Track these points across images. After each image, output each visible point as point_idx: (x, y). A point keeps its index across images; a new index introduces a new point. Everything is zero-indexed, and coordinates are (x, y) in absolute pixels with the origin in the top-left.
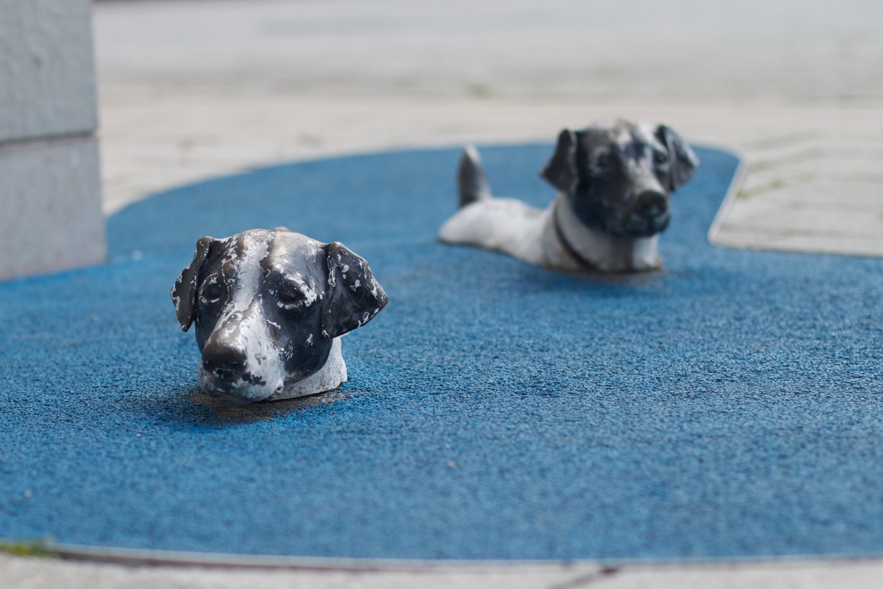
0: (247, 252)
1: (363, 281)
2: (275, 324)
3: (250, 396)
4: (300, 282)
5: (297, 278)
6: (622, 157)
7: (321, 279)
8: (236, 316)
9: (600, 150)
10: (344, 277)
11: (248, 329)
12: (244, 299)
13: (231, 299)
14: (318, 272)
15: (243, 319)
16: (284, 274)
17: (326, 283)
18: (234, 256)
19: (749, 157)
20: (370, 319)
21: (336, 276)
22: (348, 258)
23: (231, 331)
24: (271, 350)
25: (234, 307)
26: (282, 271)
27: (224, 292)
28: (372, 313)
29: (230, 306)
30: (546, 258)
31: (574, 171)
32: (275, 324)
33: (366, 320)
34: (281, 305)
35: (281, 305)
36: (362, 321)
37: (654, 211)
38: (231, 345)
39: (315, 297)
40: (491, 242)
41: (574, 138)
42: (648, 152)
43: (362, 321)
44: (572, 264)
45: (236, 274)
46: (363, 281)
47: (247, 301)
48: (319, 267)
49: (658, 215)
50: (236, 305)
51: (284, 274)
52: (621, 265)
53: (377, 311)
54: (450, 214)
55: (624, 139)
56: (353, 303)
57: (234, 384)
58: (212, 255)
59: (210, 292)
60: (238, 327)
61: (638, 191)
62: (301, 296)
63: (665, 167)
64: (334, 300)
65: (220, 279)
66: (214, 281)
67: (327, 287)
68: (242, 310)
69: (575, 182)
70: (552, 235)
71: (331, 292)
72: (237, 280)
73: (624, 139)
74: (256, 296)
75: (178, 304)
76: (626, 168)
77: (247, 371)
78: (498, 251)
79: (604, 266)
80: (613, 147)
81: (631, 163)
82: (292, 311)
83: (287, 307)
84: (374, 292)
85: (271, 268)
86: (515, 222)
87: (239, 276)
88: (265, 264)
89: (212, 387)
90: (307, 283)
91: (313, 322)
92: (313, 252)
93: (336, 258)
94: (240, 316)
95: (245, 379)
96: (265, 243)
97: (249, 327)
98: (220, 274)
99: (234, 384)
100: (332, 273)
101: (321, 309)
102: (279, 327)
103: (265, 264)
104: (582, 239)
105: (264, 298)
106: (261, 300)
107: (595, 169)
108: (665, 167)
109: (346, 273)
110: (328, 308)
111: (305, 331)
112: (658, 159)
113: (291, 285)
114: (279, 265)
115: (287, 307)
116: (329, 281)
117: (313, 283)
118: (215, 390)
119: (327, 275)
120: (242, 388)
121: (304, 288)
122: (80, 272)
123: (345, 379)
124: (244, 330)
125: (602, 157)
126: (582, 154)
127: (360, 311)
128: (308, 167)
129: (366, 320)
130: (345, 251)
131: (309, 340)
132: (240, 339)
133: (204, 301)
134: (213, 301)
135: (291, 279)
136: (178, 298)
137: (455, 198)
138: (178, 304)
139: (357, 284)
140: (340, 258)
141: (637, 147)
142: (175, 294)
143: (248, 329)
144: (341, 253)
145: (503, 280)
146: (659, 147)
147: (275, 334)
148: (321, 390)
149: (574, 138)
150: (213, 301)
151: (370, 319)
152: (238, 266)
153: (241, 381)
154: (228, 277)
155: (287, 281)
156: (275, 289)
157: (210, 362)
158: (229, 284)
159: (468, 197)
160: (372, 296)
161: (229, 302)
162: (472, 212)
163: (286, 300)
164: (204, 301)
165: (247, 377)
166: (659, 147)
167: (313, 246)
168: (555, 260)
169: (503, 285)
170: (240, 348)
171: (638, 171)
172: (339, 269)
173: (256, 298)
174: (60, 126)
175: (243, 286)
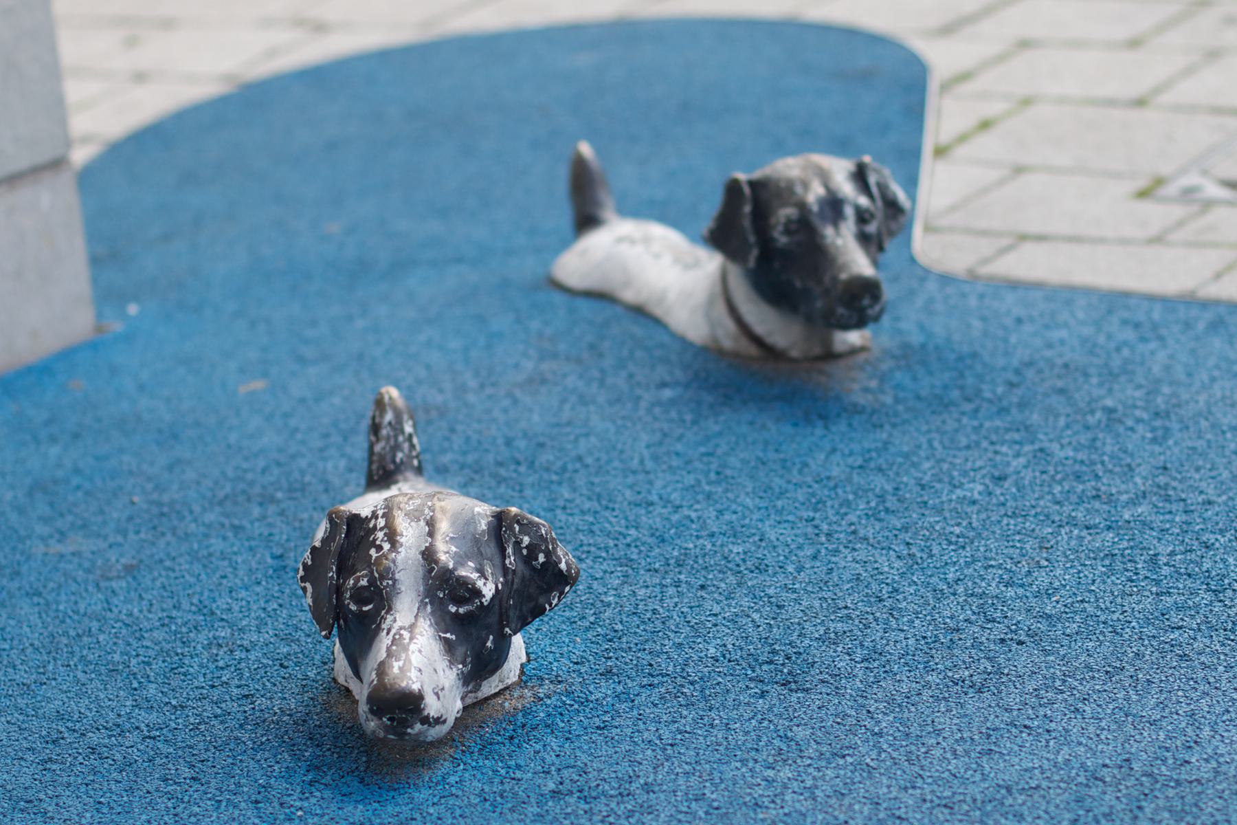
0: (403, 540)
1: (548, 554)
2: (448, 635)
3: (430, 739)
4: (475, 576)
5: (468, 572)
6: (816, 221)
7: (497, 560)
8: (401, 635)
9: (786, 213)
10: (525, 552)
11: (417, 656)
12: (406, 606)
13: (390, 609)
14: (491, 550)
15: (411, 639)
16: (455, 569)
17: (504, 565)
18: (386, 546)
19: (942, 58)
20: (559, 600)
21: (514, 554)
22: (528, 527)
23: (401, 663)
24: (448, 672)
25: (395, 620)
26: (451, 566)
27: (379, 598)
28: (562, 593)
29: (390, 618)
30: (715, 339)
31: (752, 239)
32: (448, 635)
33: (554, 602)
34: (453, 609)
35: (453, 609)
36: (550, 605)
37: (866, 301)
38: (404, 684)
39: (493, 591)
40: (629, 296)
41: (747, 190)
42: (849, 211)
43: (550, 605)
44: (753, 350)
45: (393, 574)
46: (548, 554)
47: (410, 609)
48: (493, 545)
49: (871, 306)
50: (397, 616)
51: (455, 569)
52: (817, 350)
53: (567, 589)
54: (565, 245)
55: (815, 194)
56: (538, 584)
57: (409, 730)
58: (354, 537)
59: (360, 596)
60: (407, 655)
61: (844, 276)
62: (478, 593)
63: (872, 228)
64: (515, 587)
65: (372, 582)
66: (364, 582)
67: (505, 571)
68: (407, 625)
69: (755, 253)
70: (721, 310)
71: (510, 577)
72: (395, 581)
73: (815, 194)
74: (422, 601)
75: (309, 594)
76: (823, 237)
77: (426, 713)
78: (639, 312)
79: (795, 353)
80: (802, 206)
81: (829, 231)
82: (469, 615)
83: (461, 610)
84: (563, 566)
85: (436, 562)
86: (662, 264)
87: (397, 576)
88: (428, 555)
89: (382, 735)
90: (483, 575)
91: (493, 619)
92: (483, 525)
93: (513, 530)
94: (406, 634)
95: (423, 724)
96: (422, 523)
97: (420, 651)
98: (372, 573)
99: (409, 730)
100: (510, 550)
101: (501, 601)
102: (454, 637)
103: (428, 555)
104: (764, 320)
105: (431, 603)
106: (429, 607)
107: (782, 240)
108: (872, 228)
109: (527, 547)
110: (508, 599)
111: (483, 634)
112: (862, 217)
113: (463, 583)
114: (446, 553)
115: (461, 610)
116: (507, 562)
117: (489, 570)
118: (385, 737)
119: (503, 555)
120: (420, 733)
121: (480, 583)
122: (67, 355)
123: (524, 659)
124: (416, 659)
125: (789, 222)
126: (761, 215)
127: (547, 591)
128: (318, 78)
129: (554, 602)
130: (524, 518)
131: (489, 644)
132: (413, 674)
133: (353, 607)
134: (365, 609)
135: (464, 574)
136: (308, 585)
137: (564, 215)
138: (309, 594)
139: (541, 558)
140: (517, 528)
141: (834, 206)
142: (303, 579)
143: (417, 656)
144: (518, 522)
145: (663, 385)
146: (863, 201)
147: (449, 647)
148: (501, 686)
149: (747, 190)
150: (365, 609)
151: (559, 600)
152: (394, 562)
153: (418, 727)
154: (382, 578)
155: (459, 578)
156: (444, 590)
157: (378, 708)
158: (385, 587)
159: (586, 220)
160: (561, 571)
161: (387, 613)
162: (598, 242)
163: (459, 602)
164: (353, 607)
165: (426, 720)
166: (863, 201)
167: (483, 511)
168: (728, 344)
169: (667, 393)
170: (415, 687)
171: (839, 242)
172: (518, 544)
173: (422, 605)
174: (23, 162)
175: (403, 589)
